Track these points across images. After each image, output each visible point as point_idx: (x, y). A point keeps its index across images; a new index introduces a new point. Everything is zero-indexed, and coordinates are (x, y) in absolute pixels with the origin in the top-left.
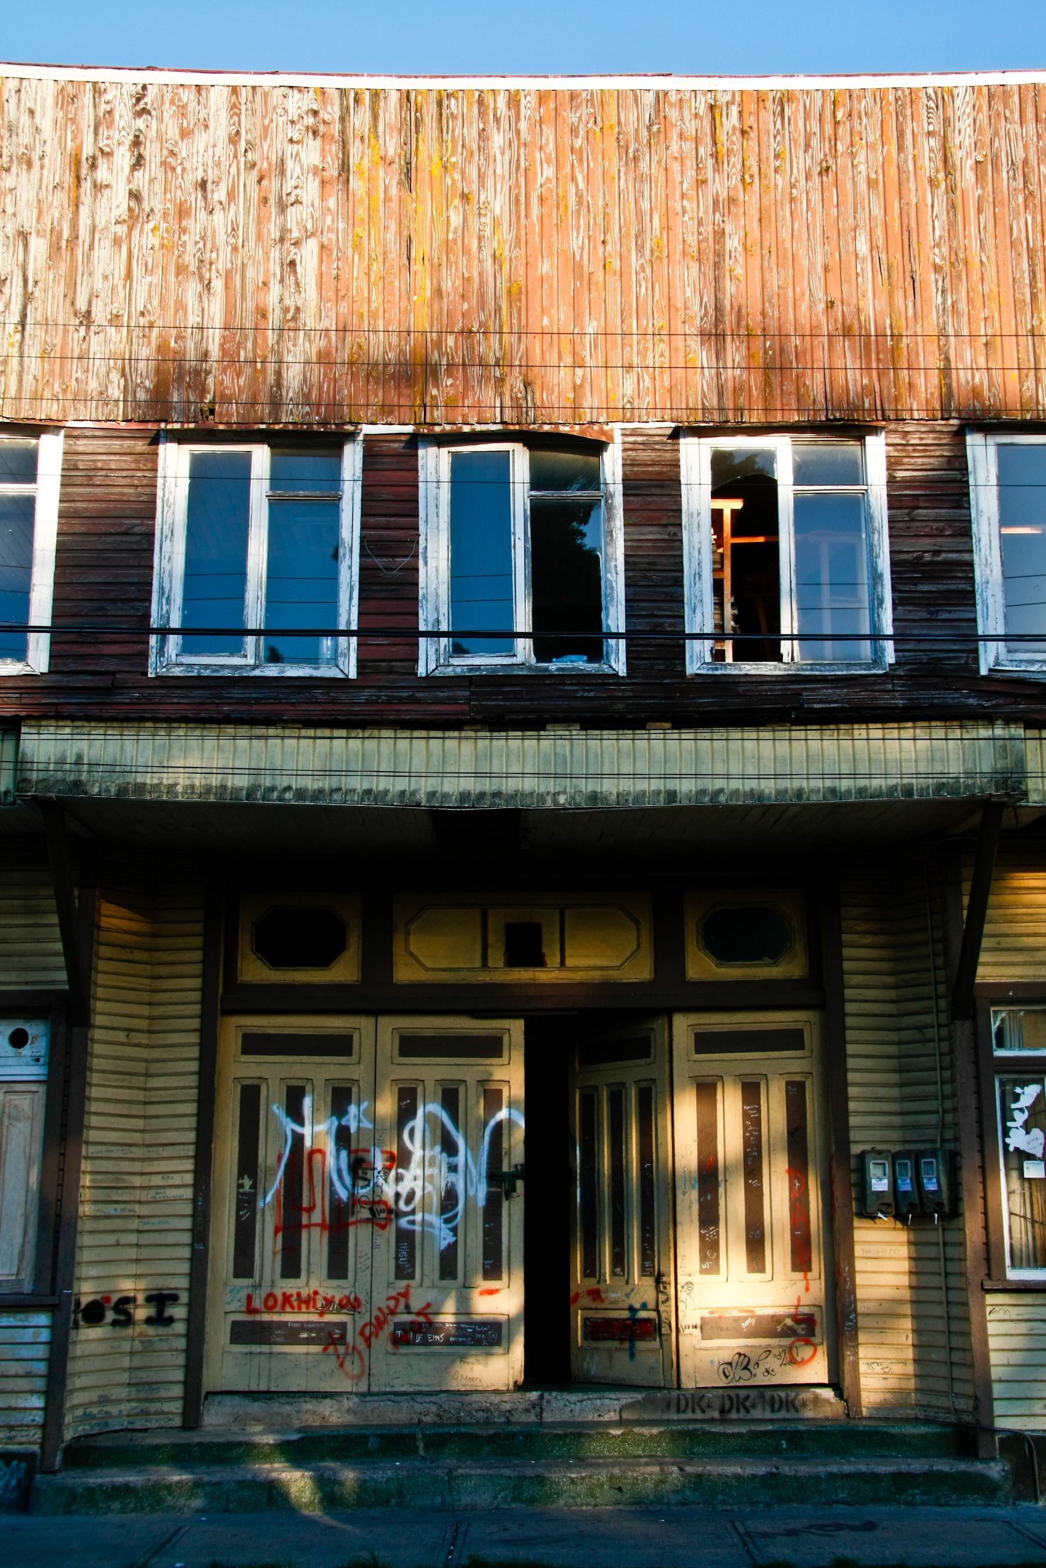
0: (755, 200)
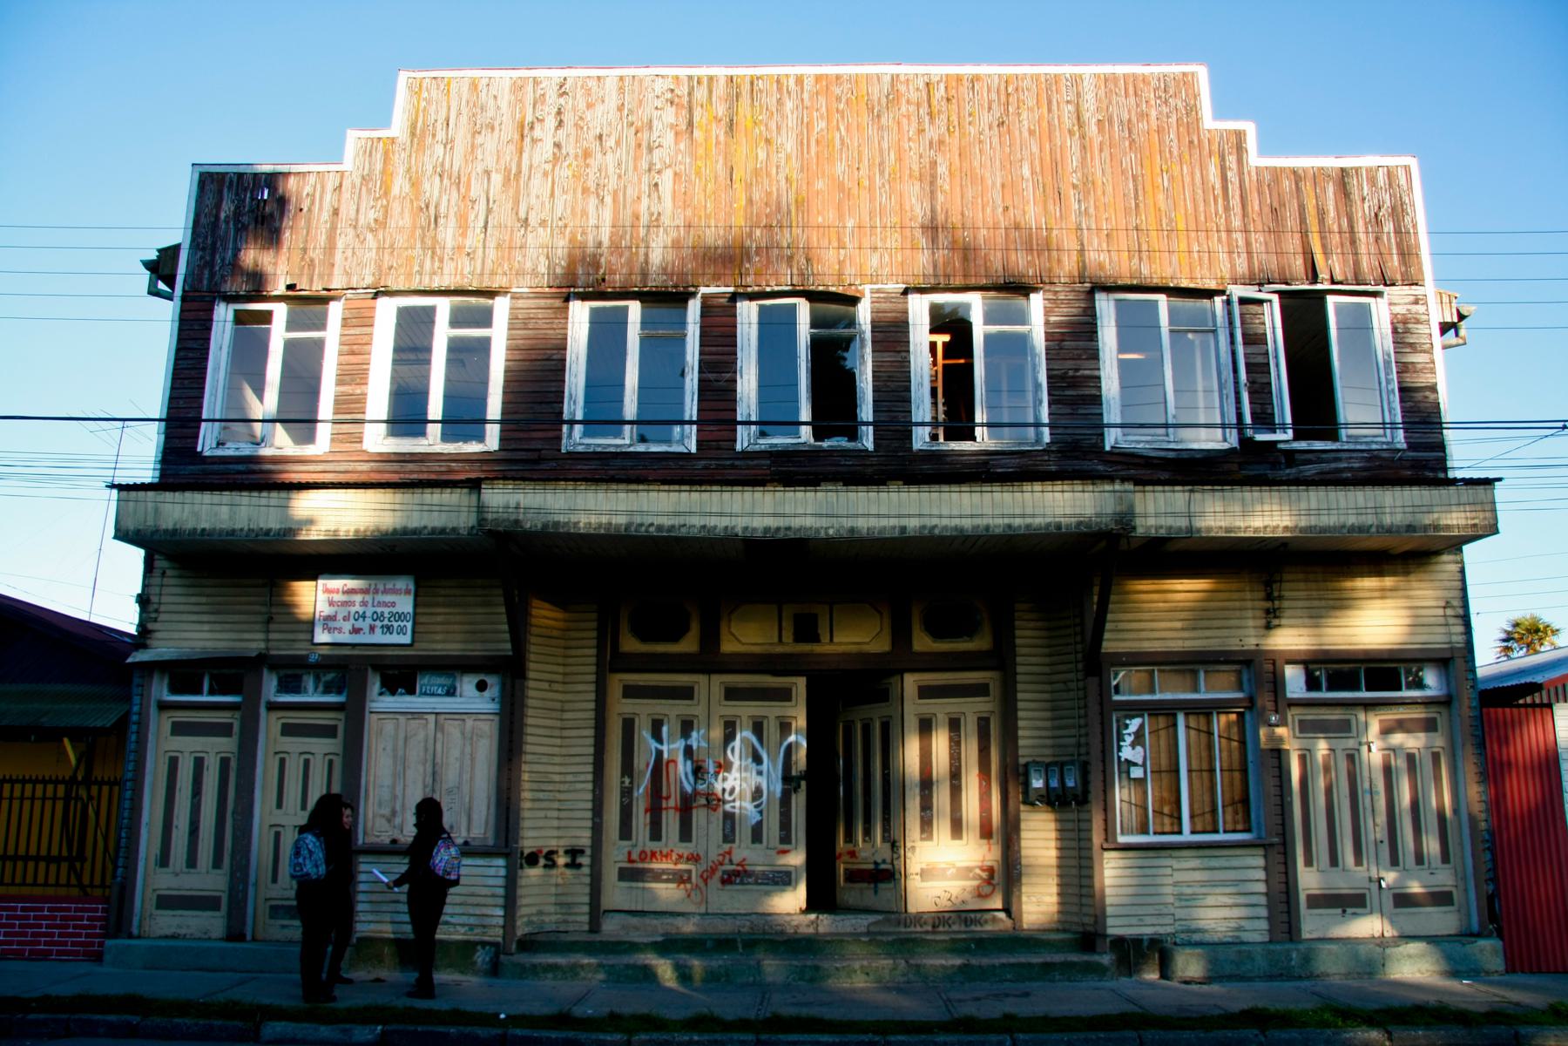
0: (956, 141)
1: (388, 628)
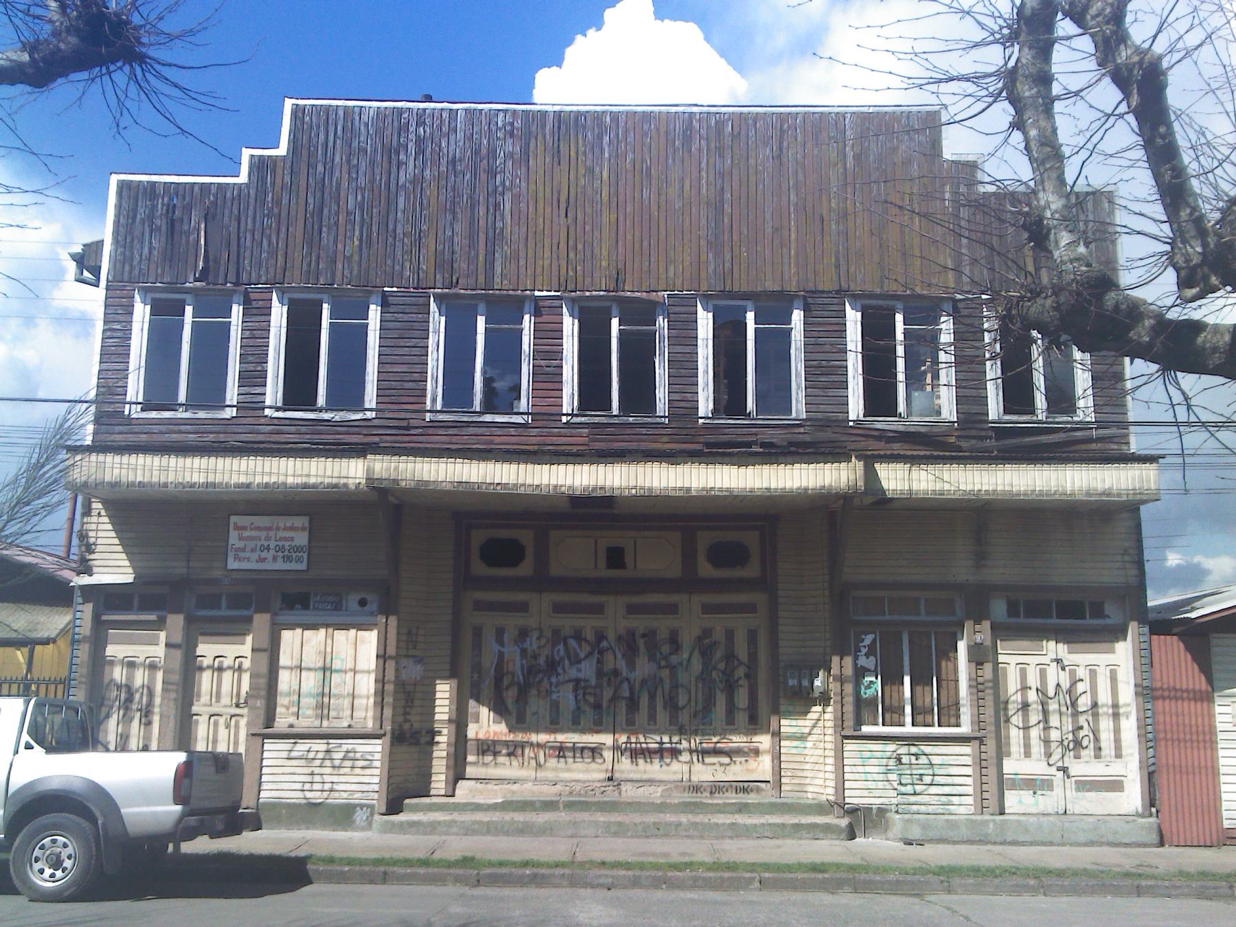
1: (288, 558)
